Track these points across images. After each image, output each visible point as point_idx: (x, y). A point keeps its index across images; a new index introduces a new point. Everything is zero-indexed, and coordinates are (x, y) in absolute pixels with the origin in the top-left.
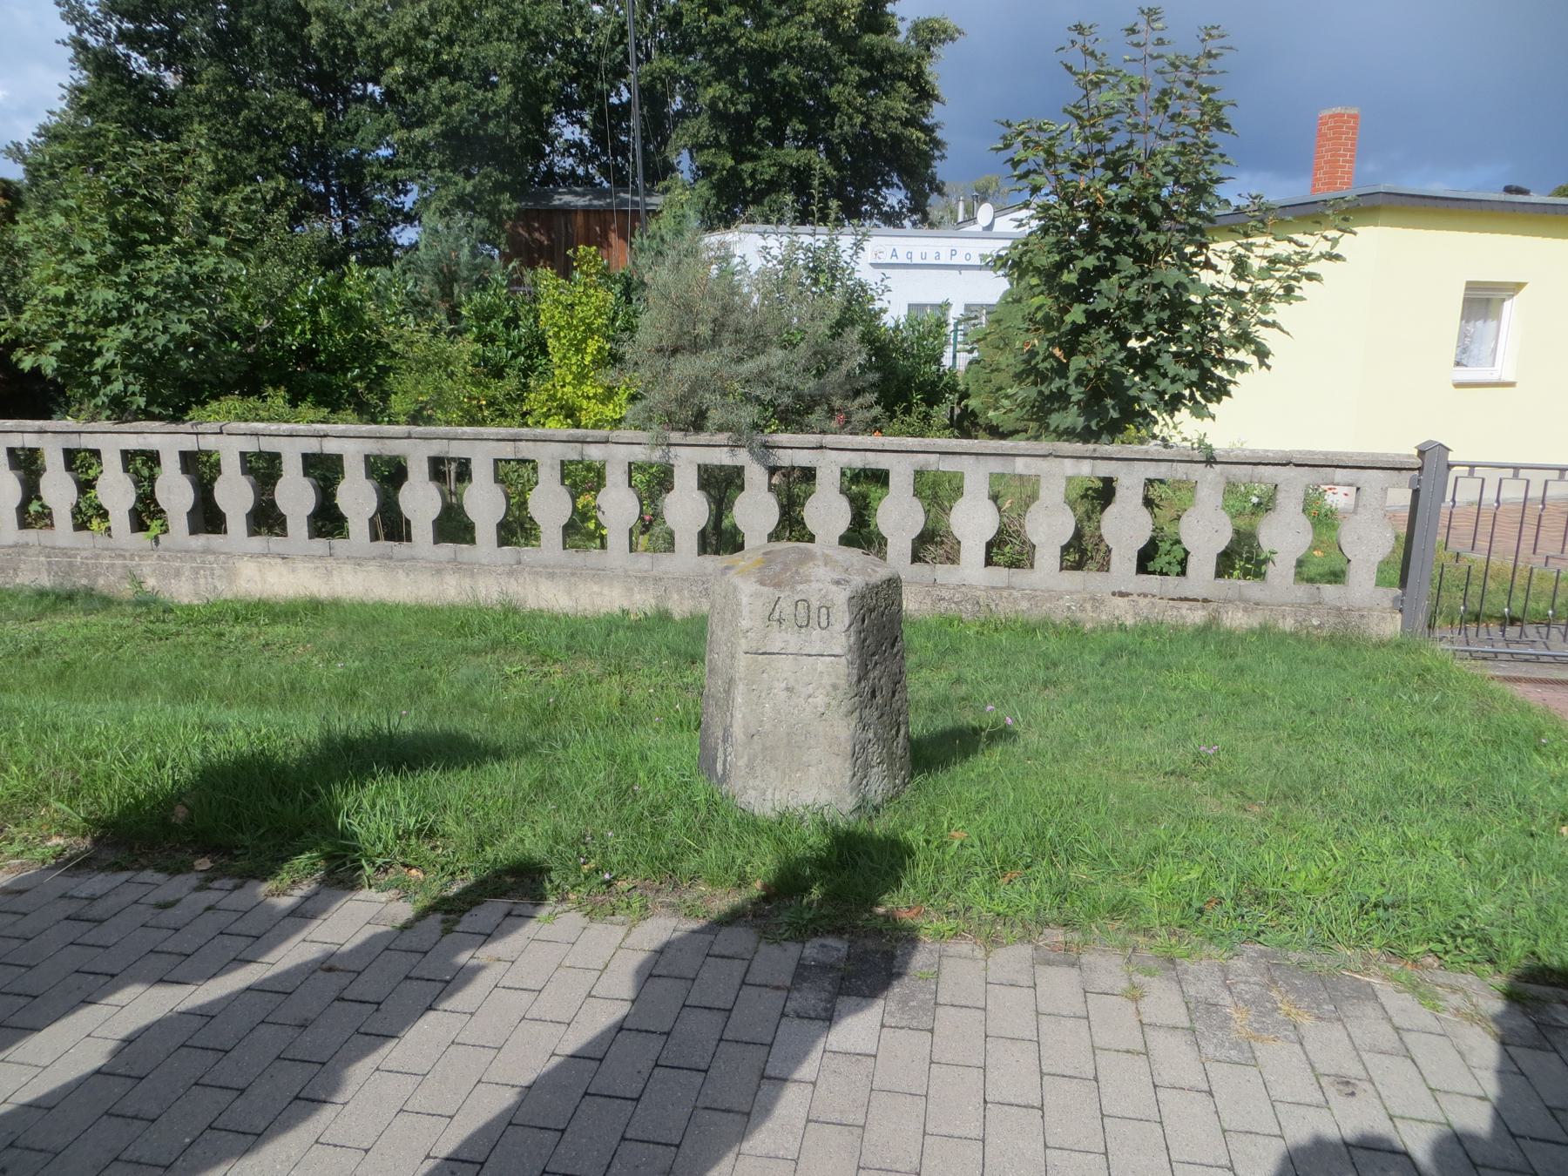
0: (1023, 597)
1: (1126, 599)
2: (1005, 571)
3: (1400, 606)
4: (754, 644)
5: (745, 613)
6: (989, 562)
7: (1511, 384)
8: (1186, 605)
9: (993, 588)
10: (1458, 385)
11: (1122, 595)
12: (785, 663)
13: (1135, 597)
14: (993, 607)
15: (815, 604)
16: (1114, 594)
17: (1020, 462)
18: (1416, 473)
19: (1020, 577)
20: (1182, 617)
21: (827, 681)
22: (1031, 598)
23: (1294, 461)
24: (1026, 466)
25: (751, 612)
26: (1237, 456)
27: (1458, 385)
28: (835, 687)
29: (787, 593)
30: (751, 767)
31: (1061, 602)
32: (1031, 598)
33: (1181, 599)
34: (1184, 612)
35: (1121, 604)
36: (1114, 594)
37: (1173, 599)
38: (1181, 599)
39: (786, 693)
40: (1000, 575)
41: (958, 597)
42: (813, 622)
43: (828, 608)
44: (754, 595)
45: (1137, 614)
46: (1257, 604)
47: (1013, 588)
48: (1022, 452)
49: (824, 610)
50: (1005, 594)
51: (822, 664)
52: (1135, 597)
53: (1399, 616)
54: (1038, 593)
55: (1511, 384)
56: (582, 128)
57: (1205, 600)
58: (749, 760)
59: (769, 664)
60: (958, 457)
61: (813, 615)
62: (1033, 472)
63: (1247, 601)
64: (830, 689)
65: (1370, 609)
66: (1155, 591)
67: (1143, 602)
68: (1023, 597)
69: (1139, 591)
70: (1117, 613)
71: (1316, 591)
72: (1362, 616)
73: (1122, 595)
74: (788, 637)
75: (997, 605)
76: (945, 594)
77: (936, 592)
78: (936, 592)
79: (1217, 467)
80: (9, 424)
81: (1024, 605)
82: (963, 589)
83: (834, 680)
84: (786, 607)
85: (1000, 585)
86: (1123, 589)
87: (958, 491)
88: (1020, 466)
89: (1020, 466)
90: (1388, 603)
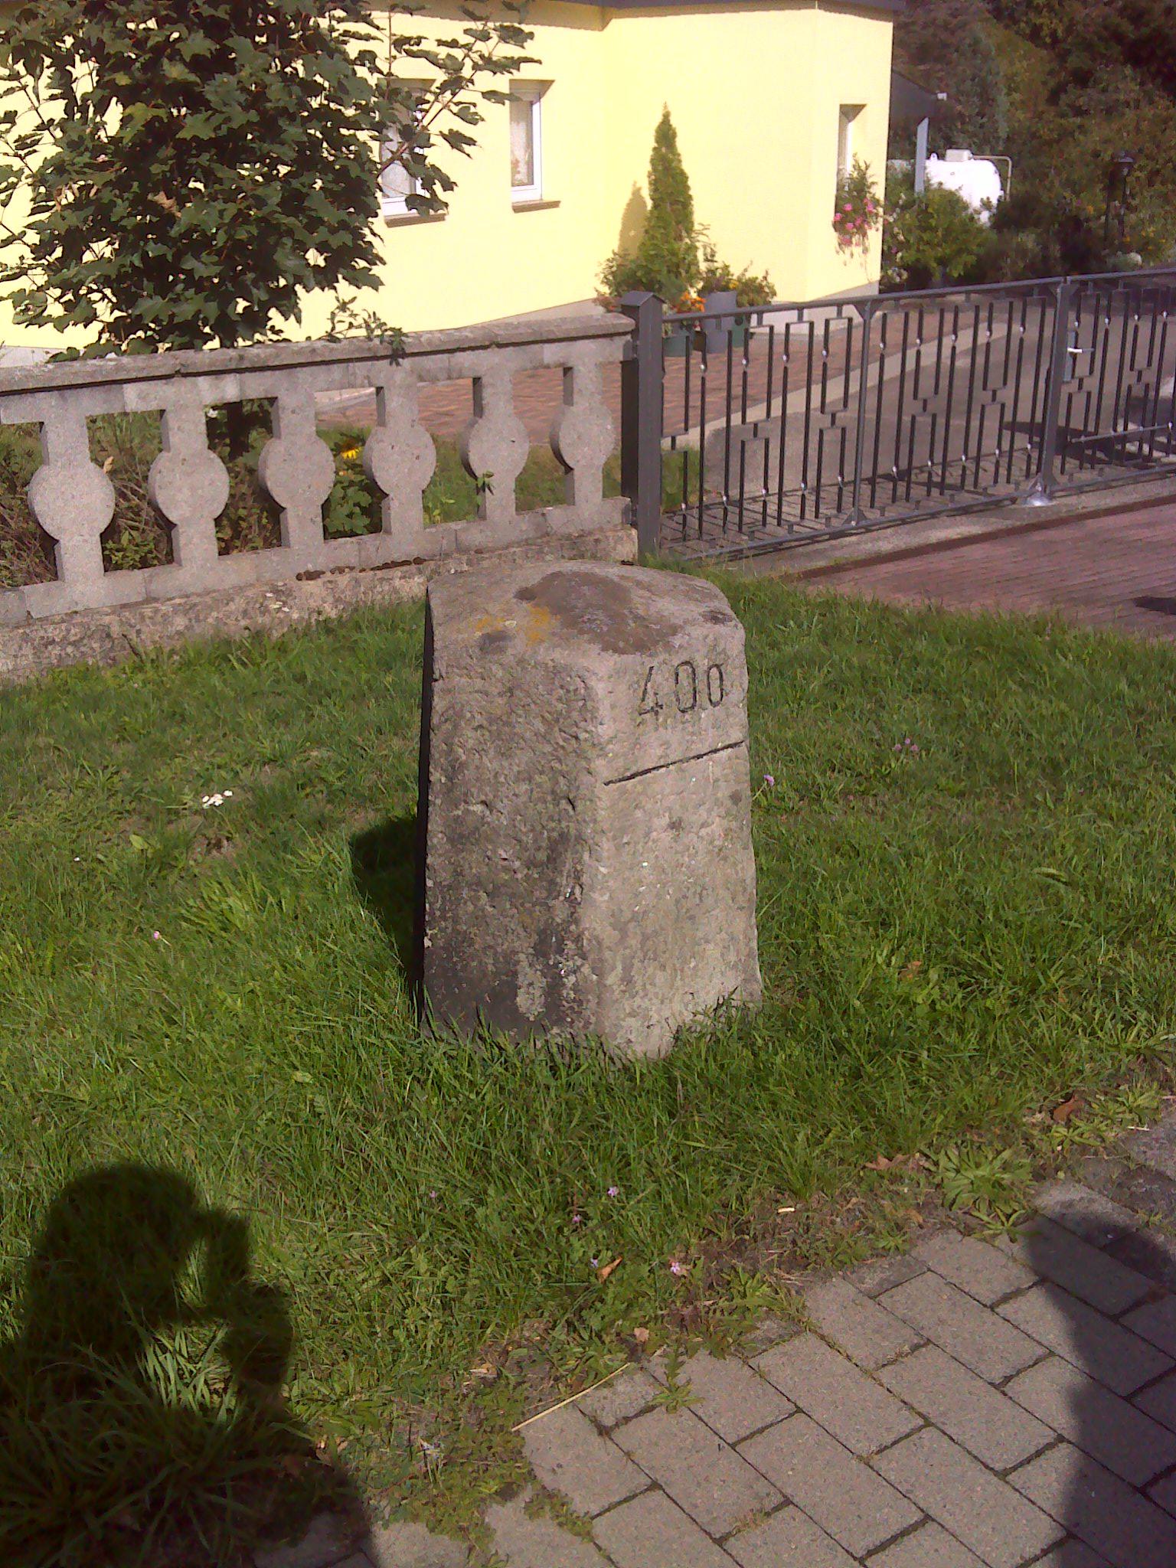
0: (175, 612)
1: (319, 581)
2: (139, 575)
3: (632, 518)
4: (621, 762)
5: (604, 711)
6: (109, 565)
7: (555, 204)
8: (397, 572)
9: (124, 606)
10: (518, 209)
11: (311, 576)
12: (664, 782)
13: (328, 576)
14: (133, 636)
15: (702, 664)
16: (299, 577)
17: (131, 391)
18: (629, 337)
19: (165, 580)
20: (396, 591)
21: (723, 793)
22: (187, 609)
23: (499, 340)
24: (142, 397)
25: (613, 707)
26: (430, 343)
27: (518, 209)
28: (735, 798)
29: (661, 658)
30: (627, 980)
31: (232, 606)
32: (187, 609)
33: (386, 566)
34: (397, 583)
35: (316, 591)
36: (299, 577)
37: (379, 568)
38: (386, 566)
39: (671, 833)
40: (132, 583)
41: (75, 633)
42: (702, 698)
43: (718, 666)
44: (619, 673)
45: (338, 600)
46: (479, 551)
47: (156, 600)
48: (133, 375)
49: (714, 672)
50: (148, 611)
51: (711, 767)
52: (328, 576)
53: (634, 532)
54: (197, 600)
55: (555, 204)
56: (1065, 91)
57: (418, 561)
58: (624, 969)
59: (644, 793)
60: (29, 399)
61: (701, 686)
62: (153, 406)
63: (466, 551)
64: (729, 803)
65: (601, 529)
66: (354, 561)
67: (343, 580)
68: (175, 612)
69: (332, 566)
70: (313, 604)
71: (541, 519)
72: (597, 541)
73: (311, 576)
74: (666, 734)
75: (139, 632)
76: (52, 632)
77: (38, 633)
78: (38, 633)
79: (406, 363)
80: (1173, 595)
81: (180, 623)
82: (78, 619)
83: (735, 788)
84: (662, 680)
85: (134, 599)
86: (310, 567)
87: (36, 458)
88: (133, 398)
89: (133, 398)
90: (617, 518)
